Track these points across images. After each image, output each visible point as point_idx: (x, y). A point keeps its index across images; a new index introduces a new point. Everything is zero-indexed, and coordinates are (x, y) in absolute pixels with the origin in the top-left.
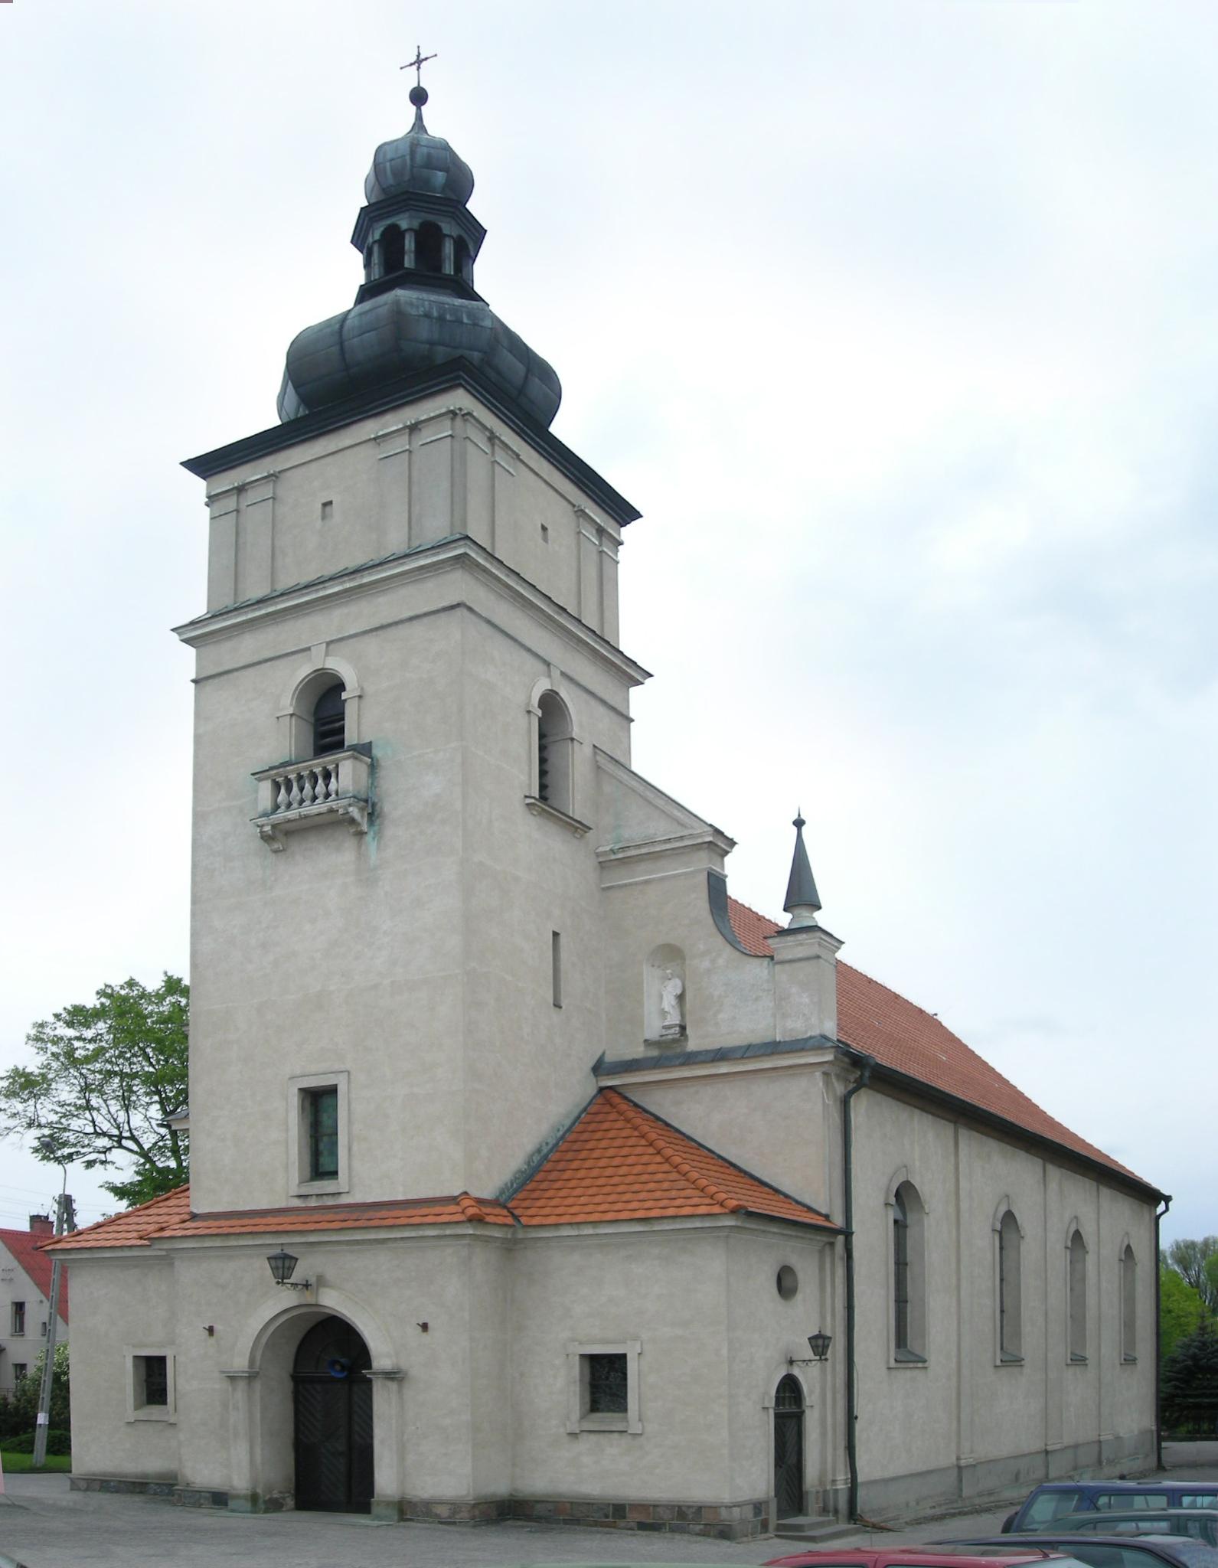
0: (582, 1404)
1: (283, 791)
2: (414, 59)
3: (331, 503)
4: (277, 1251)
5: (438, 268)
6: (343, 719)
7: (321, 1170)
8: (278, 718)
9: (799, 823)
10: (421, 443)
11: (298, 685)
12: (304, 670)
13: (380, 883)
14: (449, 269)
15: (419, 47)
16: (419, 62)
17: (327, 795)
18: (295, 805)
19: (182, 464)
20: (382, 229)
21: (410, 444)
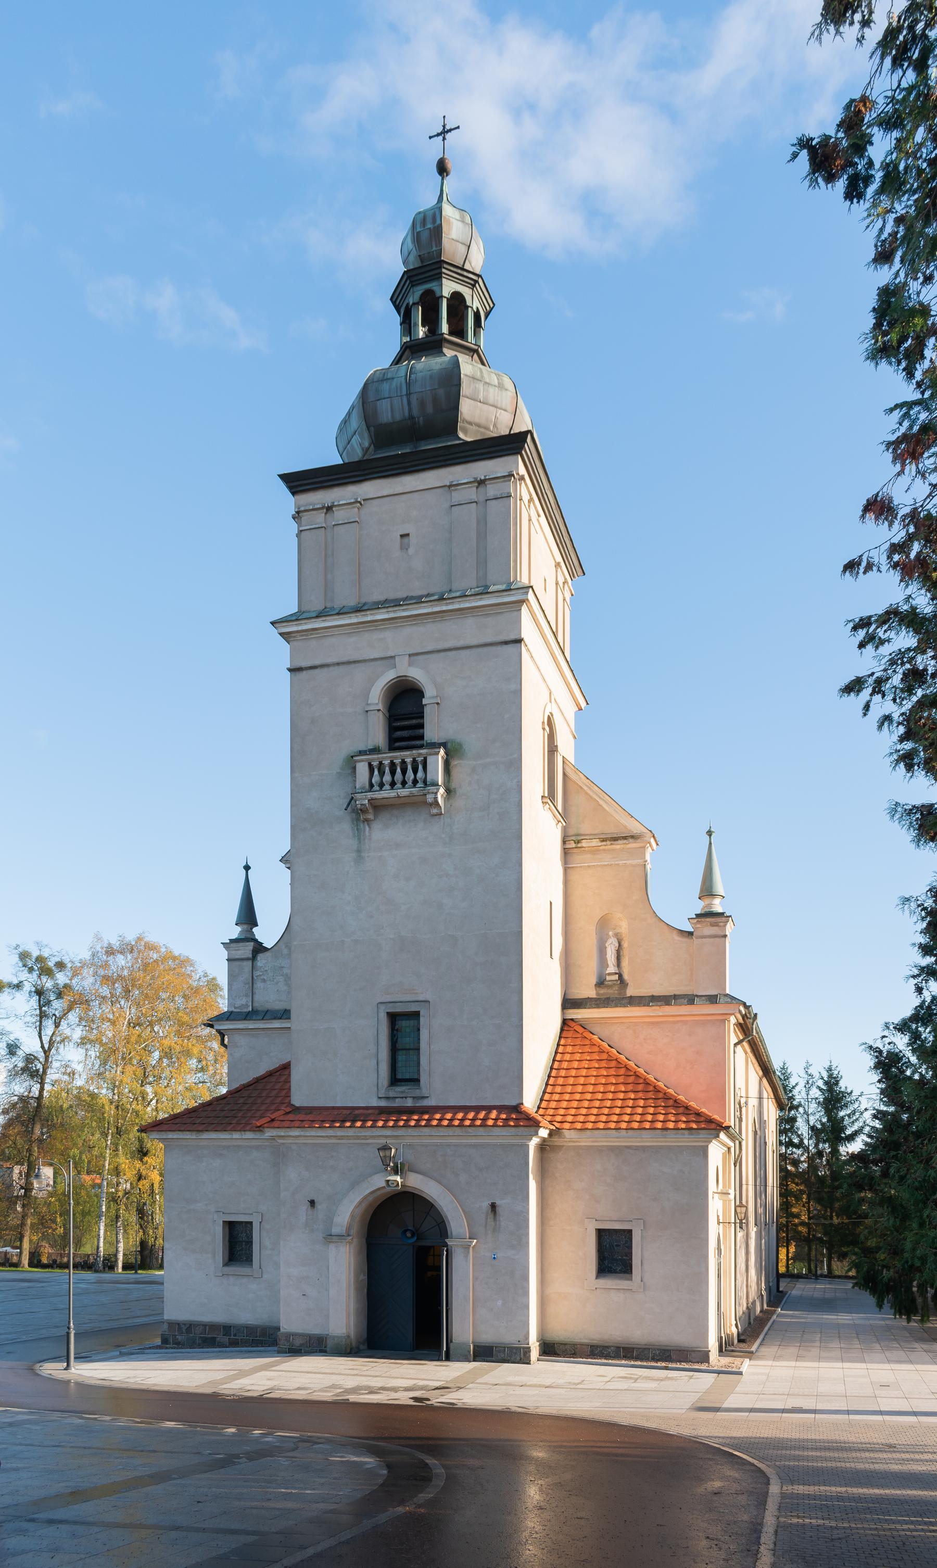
1: (376, 772)
2: (440, 130)
3: (408, 535)
6: (423, 717)
7: (399, 1076)
8: (367, 711)
10: (333, 523)
11: (383, 687)
12: (390, 676)
13: (352, 864)
16: (445, 132)
17: (415, 782)
18: (376, 788)
20: (420, 292)
21: (325, 523)
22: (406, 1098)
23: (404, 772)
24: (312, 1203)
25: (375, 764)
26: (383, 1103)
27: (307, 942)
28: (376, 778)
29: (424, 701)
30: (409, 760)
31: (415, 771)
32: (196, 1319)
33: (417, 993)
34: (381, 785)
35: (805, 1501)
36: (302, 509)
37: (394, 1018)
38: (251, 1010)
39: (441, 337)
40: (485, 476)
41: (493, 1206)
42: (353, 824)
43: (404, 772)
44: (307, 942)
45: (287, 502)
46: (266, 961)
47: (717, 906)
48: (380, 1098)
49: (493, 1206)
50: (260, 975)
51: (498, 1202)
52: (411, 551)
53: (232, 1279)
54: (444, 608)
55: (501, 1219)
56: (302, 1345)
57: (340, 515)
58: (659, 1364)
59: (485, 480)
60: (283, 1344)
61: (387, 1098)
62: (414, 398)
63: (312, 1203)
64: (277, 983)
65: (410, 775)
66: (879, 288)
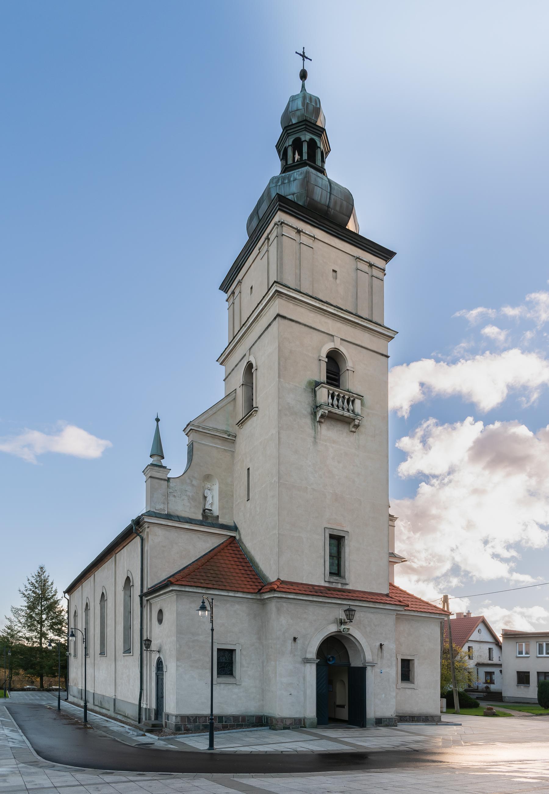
0: (413, 664)
4: (347, 607)
5: (314, 162)
8: (320, 360)
9: (158, 420)
13: (311, 444)
14: (319, 163)
15: (304, 48)
20: (293, 139)
22: (338, 583)
24: (295, 639)
26: (327, 585)
27: (288, 483)
32: (199, 713)
33: (343, 526)
36: (286, 222)
38: (167, 513)
39: (323, 170)
40: (374, 263)
41: (381, 645)
42: (312, 421)
44: (288, 483)
46: (176, 484)
48: (325, 581)
49: (381, 645)
50: (172, 492)
52: (338, 281)
53: (222, 686)
54: (360, 322)
55: (384, 652)
56: (291, 724)
59: (373, 265)
61: (329, 582)
62: (332, 197)
63: (295, 639)
64: (183, 500)
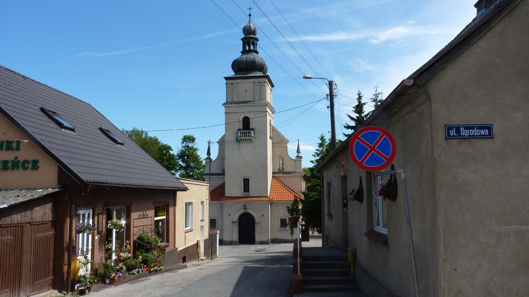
1: (241, 134)
12: (243, 116)
16: (250, 9)
17: (249, 136)
19: (224, 78)
23: (247, 134)
24: (229, 215)
25: (241, 132)
28: (241, 135)
29: (250, 121)
30: (248, 132)
31: (249, 134)
34: (242, 136)
35: (495, 229)
37: (245, 180)
43: (247, 134)
45: (225, 81)
47: (300, 155)
49: (263, 215)
51: (264, 214)
52: (247, 93)
57: (234, 85)
58: (173, 189)
60: (224, 243)
63: (229, 215)
65: (248, 135)
66: (328, 107)
